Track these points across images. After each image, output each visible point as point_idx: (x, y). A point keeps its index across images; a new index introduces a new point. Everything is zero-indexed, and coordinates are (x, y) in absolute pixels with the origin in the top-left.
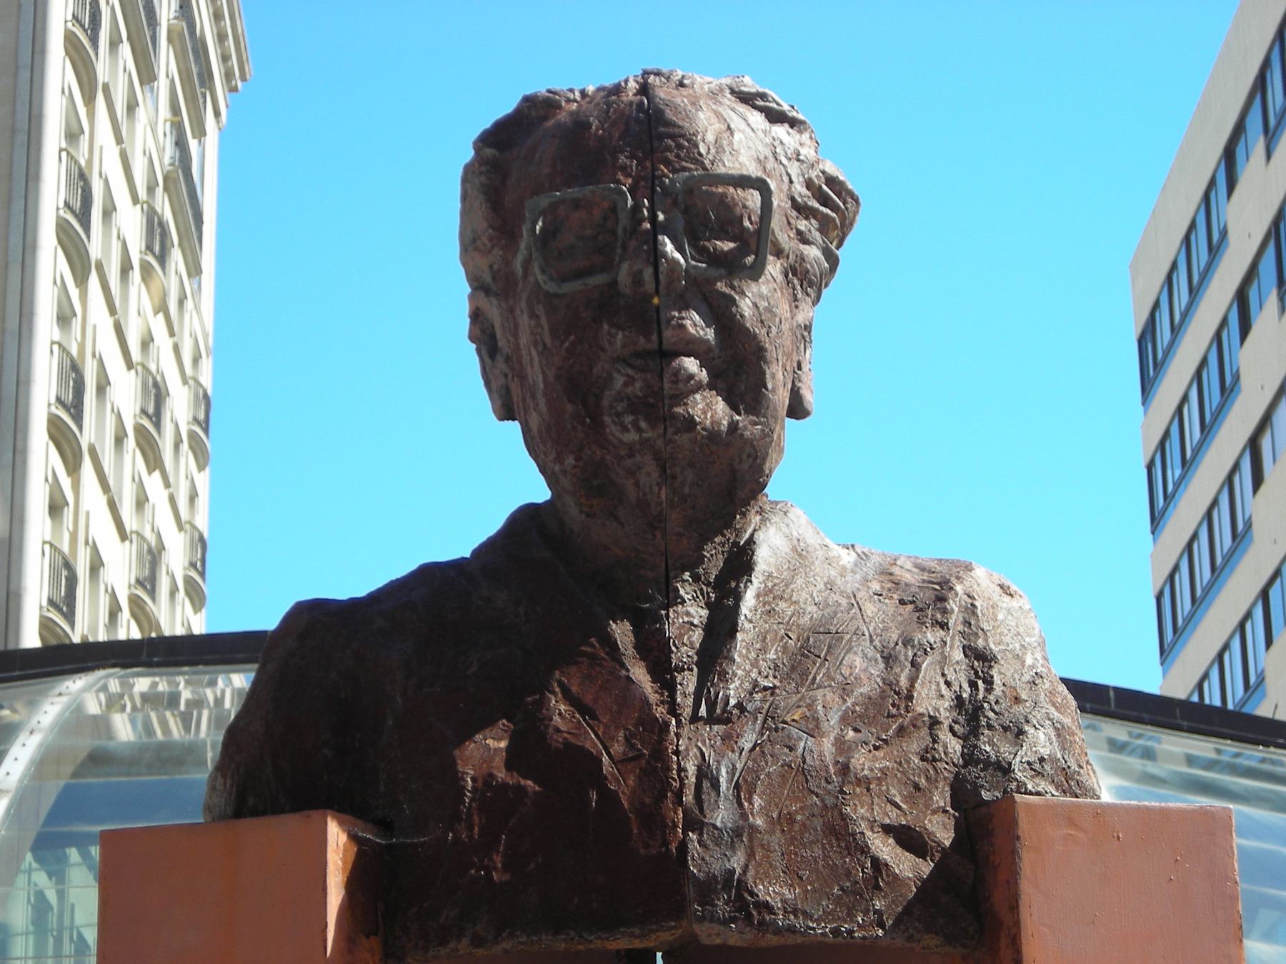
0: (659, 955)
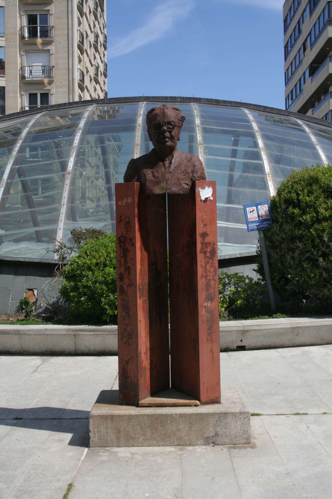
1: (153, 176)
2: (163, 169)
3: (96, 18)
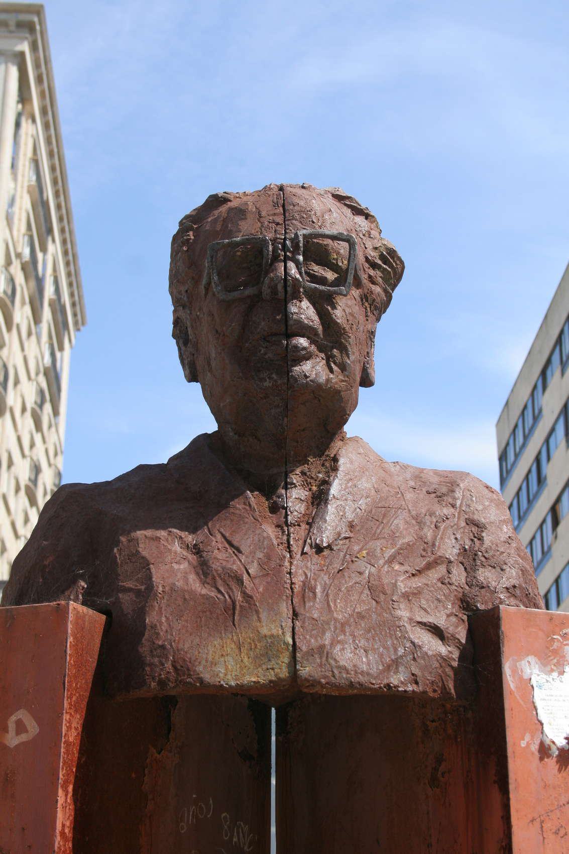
0: (273, 710)
1: (203, 569)
2: (270, 530)
3: (38, 426)
